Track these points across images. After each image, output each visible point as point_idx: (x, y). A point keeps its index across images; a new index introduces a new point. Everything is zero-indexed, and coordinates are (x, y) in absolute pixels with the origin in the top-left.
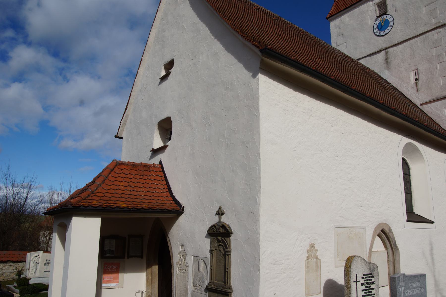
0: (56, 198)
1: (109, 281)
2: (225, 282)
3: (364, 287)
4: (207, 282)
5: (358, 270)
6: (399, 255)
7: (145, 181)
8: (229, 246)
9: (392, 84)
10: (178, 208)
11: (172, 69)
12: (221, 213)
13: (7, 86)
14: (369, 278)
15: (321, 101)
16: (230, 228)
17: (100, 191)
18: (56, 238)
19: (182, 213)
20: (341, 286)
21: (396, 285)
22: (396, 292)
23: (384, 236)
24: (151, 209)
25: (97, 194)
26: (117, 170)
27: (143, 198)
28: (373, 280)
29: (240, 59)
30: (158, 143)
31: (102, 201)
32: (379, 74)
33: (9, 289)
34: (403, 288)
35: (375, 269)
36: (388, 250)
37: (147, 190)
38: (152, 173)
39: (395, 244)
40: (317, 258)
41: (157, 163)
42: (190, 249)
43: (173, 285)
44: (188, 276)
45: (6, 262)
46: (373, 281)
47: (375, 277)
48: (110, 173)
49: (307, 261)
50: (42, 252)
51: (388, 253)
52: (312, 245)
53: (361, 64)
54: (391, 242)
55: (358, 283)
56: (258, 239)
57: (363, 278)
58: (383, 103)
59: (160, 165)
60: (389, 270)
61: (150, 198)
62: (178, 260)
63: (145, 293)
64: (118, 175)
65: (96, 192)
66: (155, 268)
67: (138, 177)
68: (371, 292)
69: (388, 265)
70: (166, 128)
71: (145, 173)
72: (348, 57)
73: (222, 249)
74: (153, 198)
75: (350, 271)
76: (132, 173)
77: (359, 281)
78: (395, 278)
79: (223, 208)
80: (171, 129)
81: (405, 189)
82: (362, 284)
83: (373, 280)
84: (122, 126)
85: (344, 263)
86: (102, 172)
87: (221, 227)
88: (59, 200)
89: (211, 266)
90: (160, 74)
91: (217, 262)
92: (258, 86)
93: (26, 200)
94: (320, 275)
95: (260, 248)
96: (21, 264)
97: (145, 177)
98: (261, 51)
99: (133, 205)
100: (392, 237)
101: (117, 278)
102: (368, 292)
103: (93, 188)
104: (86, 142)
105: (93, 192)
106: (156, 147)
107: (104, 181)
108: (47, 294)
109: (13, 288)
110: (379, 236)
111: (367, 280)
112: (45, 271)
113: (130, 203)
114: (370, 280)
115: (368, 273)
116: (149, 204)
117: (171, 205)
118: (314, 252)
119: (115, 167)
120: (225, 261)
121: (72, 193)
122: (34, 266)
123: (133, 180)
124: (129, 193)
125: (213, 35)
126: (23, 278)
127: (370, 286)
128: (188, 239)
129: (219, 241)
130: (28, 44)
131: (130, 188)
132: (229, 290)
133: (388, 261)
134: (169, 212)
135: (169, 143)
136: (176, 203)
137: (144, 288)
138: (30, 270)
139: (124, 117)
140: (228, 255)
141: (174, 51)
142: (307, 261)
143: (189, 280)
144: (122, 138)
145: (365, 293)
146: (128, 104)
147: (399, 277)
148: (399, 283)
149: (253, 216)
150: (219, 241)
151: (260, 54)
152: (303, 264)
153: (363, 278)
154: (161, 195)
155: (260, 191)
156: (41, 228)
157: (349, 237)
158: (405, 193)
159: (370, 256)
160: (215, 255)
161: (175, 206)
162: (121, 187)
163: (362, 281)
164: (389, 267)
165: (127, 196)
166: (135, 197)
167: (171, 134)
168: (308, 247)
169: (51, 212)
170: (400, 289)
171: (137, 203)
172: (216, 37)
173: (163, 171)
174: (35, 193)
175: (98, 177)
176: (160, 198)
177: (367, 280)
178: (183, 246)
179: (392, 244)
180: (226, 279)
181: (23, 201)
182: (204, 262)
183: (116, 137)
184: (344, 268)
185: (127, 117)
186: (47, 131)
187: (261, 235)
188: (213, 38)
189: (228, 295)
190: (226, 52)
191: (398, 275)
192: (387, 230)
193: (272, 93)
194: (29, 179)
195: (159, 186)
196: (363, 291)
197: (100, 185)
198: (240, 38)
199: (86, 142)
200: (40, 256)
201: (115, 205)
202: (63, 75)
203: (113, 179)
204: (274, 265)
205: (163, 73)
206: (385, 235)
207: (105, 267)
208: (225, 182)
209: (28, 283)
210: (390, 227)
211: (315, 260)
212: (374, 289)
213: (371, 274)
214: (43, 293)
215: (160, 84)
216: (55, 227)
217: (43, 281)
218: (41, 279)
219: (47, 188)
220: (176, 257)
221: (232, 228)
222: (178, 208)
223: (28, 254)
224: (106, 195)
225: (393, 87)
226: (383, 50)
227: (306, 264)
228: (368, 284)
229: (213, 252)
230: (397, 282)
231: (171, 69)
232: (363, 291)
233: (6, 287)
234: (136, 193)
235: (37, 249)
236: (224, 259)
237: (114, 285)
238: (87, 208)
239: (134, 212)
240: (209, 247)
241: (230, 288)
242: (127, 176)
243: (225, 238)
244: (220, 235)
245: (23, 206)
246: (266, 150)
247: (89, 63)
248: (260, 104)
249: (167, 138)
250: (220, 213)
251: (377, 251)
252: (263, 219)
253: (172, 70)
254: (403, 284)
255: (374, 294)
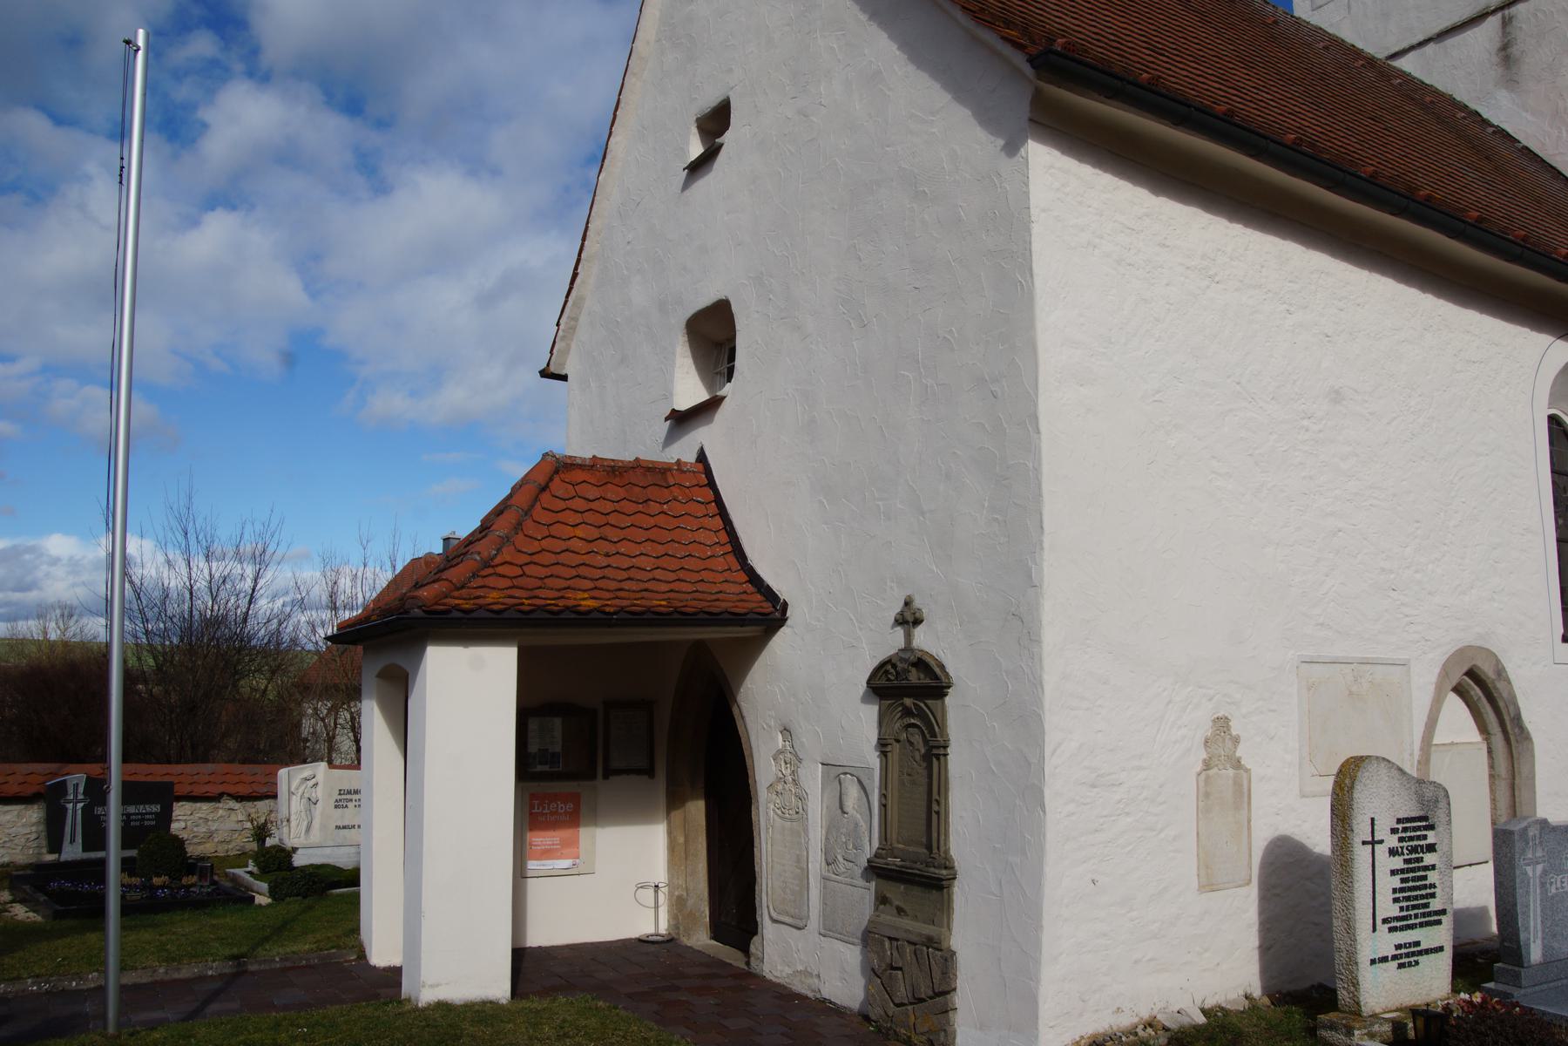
0: (348, 591)
1: (547, 854)
2: (929, 847)
3: (1398, 862)
4: (869, 846)
5: (1380, 806)
6: (1533, 756)
7: (652, 521)
8: (943, 727)
9: (1525, 142)
10: (767, 607)
11: (727, 134)
12: (910, 619)
13: (193, 223)
14: (1418, 832)
15: (1246, 225)
16: (942, 667)
17: (508, 558)
18: (373, 717)
19: (781, 621)
20: (1319, 858)
21: (1513, 858)
22: (1514, 880)
23: (1476, 691)
24: (676, 611)
25: (500, 570)
26: (558, 487)
27: (650, 575)
28: (1431, 837)
29: (959, 89)
30: (689, 390)
31: (518, 593)
32: (1473, 106)
33: (235, 879)
34: (1539, 868)
35: (1437, 801)
36: (1493, 739)
37: (661, 550)
38: (676, 492)
39: (1517, 719)
40: (1237, 764)
41: (690, 457)
42: (811, 742)
43: (757, 860)
44: (806, 831)
45: (216, 798)
46: (1430, 840)
47: (1440, 829)
48: (536, 499)
49: (1203, 776)
50: (323, 765)
51: (1490, 752)
52: (1222, 723)
53: (1402, 74)
54: (1504, 712)
55: (1377, 847)
56: (1038, 701)
57: (1394, 831)
58: (1480, 220)
59: (701, 466)
60: (1494, 808)
61: (672, 576)
62: (772, 779)
63: (666, 890)
64: (562, 505)
65: (498, 560)
66: (697, 810)
67: (629, 507)
68: (1425, 878)
69: (1492, 791)
70: (713, 336)
71: (652, 492)
72: (1355, 53)
73: (917, 739)
74: (681, 574)
75: (1350, 807)
76: (609, 496)
77: (1381, 842)
78: (1511, 833)
79: (917, 603)
80: (733, 339)
81: (1557, 528)
82: (1393, 852)
83: (1431, 837)
84: (563, 338)
85: (1329, 783)
86: (510, 497)
87: (914, 665)
88: (360, 596)
89: (883, 796)
90: (684, 151)
91: (902, 783)
92: (1027, 185)
93: (250, 602)
94: (1249, 821)
95: (1043, 733)
96: (263, 806)
97: (654, 508)
98: (1031, 60)
99: (617, 602)
100: (1505, 695)
101: (575, 843)
102: (1414, 879)
103: (485, 548)
104: (455, 396)
105: (487, 564)
106: (683, 404)
107: (518, 526)
108: (357, 895)
109: (248, 877)
110: (1459, 690)
111: (1411, 839)
112: (338, 827)
113: (608, 595)
114: (1419, 838)
115: (1414, 814)
116: (672, 595)
117: (744, 597)
118: (1229, 744)
119: (551, 479)
120: (930, 776)
121: (399, 568)
122: (306, 810)
123: (612, 519)
124: (601, 560)
125: (864, 9)
126: (274, 847)
127: (1420, 860)
128: (805, 709)
129: (907, 712)
130: (261, 76)
131: (604, 547)
132: (944, 872)
133: (1492, 777)
134: (738, 619)
135: (727, 390)
136: (759, 591)
137: (660, 874)
138: (293, 824)
139: (569, 304)
140: (938, 757)
141: (731, 70)
142: (1203, 776)
143: (812, 842)
144: (564, 378)
145: (1403, 880)
146: (578, 261)
147: (1525, 829)
148: (1523, 851)
149: (1020, 624)
150: (907, 712)
151: (1028, 70)
152: (1190, 787)
153: (1394, 831)
154: (708, 564)
155: (1041, 542)
156: (305, 689)
157: (1351, 693)
158: (1559, 541)
159: (1425, 760)
160: (896, 757)
161: (756, 602)
162: (577, 544)
163: (1393, 841)
164: (1493, 800)
165: (598, 574)
166: (625, 575)
167: (732, 358)
168: (1206, 729)
169: (347, 636)
170: (1529, 869)
171: (632, 595)
172: (874, 16)
173: (711, 484)
174: (277, 577)
175: (499, 511)
176: (705, 575)
177: (1411, 839)
178: (786, 731)
179: (1506, 718)
180: (935, 835)
181: (244, 603)
182: (860, 781)
183: (545, 374)
184: (1329, 799)
185: (579, 305)
186: (311, 367)
187: (1048, 688)
188: (863, 17)
189: (940, 888)
190: (911, 68)
191: (1524, 824)
192: (1487, 670)
193: (1076, 205)
194: (258, 527)
195: (702, 536)
196: (1393, 873)
197: (506, 540)
198: (959, 14)
199: (455, 396)
200: (320, 777)
201: (561, 603)
202: (371, 174)
203: (545, 518)
204: (1093, 786)
205: (696, 149)
206: (1480, 687)
207: (532, 807)
208: (923, 513)
209: (290, 863)
210: (1498, 661)
211: (1231, 772)
212: (1433, 867)
213: (1424, 818)
214: (342, 895)
215: (687, 185)
216: (369, 681)
217: (341, 858)
218: (328, 851)
219: (315, 560)
220: (765, 769)
221: (950, 669)
222: (767, 607)
223: (283, 773)
224: (528, 570)
225: (1527, 151)
226: (1494, 12)
227: (1202, 784)
228: (1414, 850)
229: (889, 748)
230: (1518, 845)
231: (721, 134)
232: (1393, 873)
233: (226, 875)
234: (627, 563)
235: (298, 756)
236: (925, 773)
237: (566, 863)
238: (474, 615)
239: (623, 623)
240: (876, 732)
241: (948, 865)
242: (594, 505)
243: (929, 702)
244: (909, 690)
245: (245, 620)
246: (1061, 404)
247: (462, 132)
248: (1036, 247)
249: (719, 373)
250: (909, 619)
251: (1452, 744)
252: (1050, 636)
253: (728, 138)
254: (1539, 854)
255: (1433, 886)
